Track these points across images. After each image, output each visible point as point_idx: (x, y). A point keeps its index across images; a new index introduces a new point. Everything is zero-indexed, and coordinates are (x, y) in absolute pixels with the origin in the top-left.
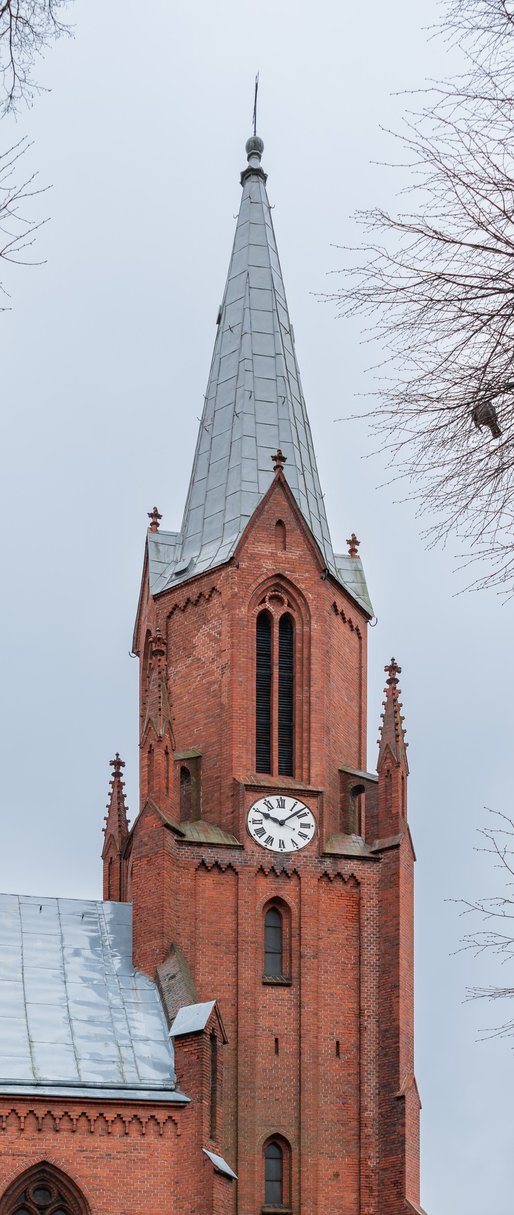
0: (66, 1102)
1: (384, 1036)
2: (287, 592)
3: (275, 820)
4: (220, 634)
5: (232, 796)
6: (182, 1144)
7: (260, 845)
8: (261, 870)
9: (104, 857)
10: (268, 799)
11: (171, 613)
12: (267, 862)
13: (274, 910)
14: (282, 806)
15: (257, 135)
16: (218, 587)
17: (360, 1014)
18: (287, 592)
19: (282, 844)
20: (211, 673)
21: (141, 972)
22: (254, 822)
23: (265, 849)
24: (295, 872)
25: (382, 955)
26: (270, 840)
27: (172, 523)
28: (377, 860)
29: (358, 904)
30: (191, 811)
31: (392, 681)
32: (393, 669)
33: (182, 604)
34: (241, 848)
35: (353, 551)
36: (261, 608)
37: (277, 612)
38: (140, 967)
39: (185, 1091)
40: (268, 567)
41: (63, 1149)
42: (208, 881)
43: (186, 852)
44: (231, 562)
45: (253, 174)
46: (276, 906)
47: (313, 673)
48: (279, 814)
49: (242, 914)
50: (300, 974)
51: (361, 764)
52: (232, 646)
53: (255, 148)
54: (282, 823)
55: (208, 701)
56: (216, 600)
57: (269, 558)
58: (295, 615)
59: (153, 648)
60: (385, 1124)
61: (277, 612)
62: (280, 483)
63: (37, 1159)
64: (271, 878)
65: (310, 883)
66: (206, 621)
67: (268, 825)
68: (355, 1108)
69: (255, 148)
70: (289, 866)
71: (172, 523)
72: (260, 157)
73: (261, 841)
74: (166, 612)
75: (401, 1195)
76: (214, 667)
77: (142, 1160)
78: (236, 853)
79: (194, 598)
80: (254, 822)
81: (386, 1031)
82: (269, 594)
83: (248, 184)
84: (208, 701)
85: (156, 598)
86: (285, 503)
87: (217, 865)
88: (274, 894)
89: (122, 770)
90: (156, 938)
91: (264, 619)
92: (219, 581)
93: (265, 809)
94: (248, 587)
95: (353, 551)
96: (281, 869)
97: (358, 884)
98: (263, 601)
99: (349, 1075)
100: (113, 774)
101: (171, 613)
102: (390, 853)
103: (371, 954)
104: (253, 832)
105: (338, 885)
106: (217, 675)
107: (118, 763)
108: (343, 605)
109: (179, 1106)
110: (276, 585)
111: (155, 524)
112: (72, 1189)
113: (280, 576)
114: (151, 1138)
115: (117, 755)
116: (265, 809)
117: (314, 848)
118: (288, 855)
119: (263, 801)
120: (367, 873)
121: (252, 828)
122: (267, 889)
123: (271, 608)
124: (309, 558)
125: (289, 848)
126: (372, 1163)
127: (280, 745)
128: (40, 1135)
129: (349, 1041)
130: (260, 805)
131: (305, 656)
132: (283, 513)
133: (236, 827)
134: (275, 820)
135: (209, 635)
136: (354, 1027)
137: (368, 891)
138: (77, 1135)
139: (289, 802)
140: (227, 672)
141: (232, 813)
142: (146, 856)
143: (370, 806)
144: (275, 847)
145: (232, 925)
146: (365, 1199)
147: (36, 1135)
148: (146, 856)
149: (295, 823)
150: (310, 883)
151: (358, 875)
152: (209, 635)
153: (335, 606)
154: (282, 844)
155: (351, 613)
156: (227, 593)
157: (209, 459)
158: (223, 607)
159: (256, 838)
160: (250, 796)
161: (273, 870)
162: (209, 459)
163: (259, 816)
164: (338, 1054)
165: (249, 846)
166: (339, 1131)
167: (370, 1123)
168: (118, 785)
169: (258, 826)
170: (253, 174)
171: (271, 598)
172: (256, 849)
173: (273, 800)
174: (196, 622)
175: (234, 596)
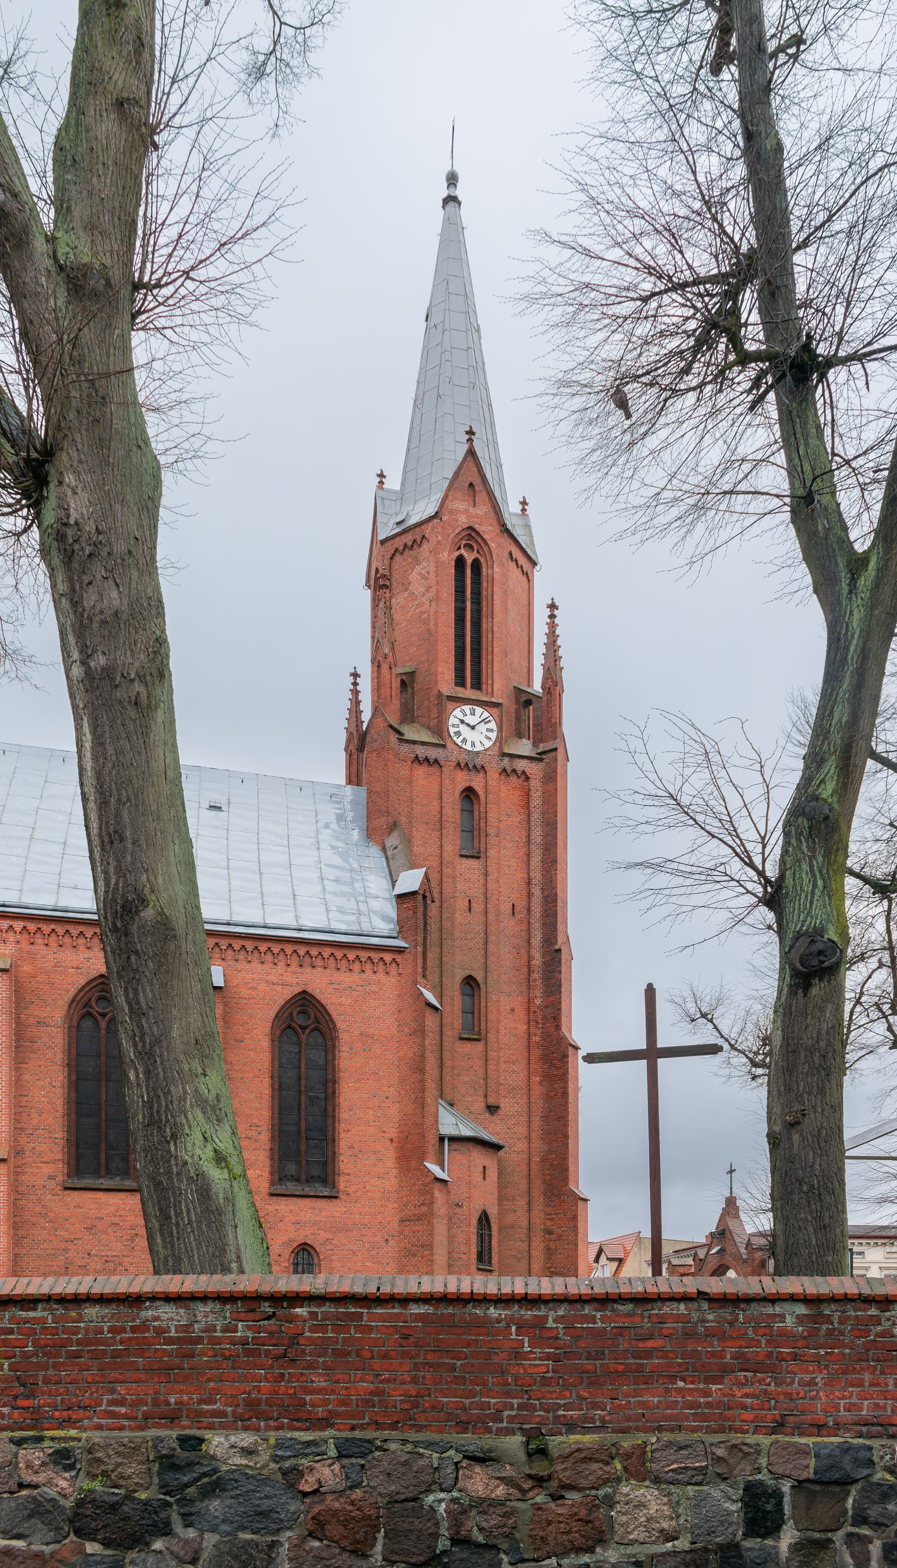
2: (477, 541)
3: (468, 725)
6: (403, 981)
8: (459, 764)
13: (467, 797)
14: (473, 713)
17: (529, 883)
18: (477, 541)
19: (473, 744)
22: (453, 726)
24: (483, 767)
25: (546, 835)
26: (465, 741)
27: (393, 483)
28: (541, 760)
29: (528, 794)
30: (408, 715)
31: (552, 617)
32: (553, 606)
33: (401, 548)
35: (524, 510)
36: (457, 553)
37: (469, 557)
39: (405, 939)
40: (463, 521)
41: (319, 981)
42: (420, 772)
43: (405, 748)
44: (436, 515)
45: (451, 200)
46: (469, 794)
51: (529, 683)
53: (452, 179)
54: (473, 728)
57: (465, 512)
58: (482, 560)
59: (380, 583)
61: (469, 557)
62: (471, 453)
63: (298, 989)
64: (465, 772)
66: (418, 563)
67: (463, 729)
68: (525, 958)
69: (452, 179)
70: (478, 762)
71: (393, 483)
73: (458, 741)
75: (558, 1027)
77: (375, 992)
78: (441, 750)
79: (410, 543)
80: (453, 726)
82: (464, 542)
83: (447, 208)
85: (383, 542)
86: (475, 469)
89: (358, 680)
91: (460, 562)
92: (427, 530)
95: (524, 510)
96: (471, 765)
97: (527, 778)
98: (459, 548)
102: (550, 755)
103: (537, 834)
105: (513, 779)
107: (355, 675)
108: (517, 554)
109: (399, 951)
110: (470, 535)
111: (381, 483)
113: (471, 528)
114: (381, 976)
116: (461, 716)
117: (496, 749)
118: (478, 753)
120: (534, 770)
121: (452, 730)
122: (462, 780)
123: (465, 554)
124: (492, 514)
125: (479, 748)
126: (538, 1002)
127: (472, 662)
129: (521, 905)
130: (457, 712)
132: (473, 478)
133: (440, 729)
134: (468, 725)
135: (420, 574)
136: (524, 893)
139: (479, 710)
143: (535, 716)
144: (468, 747)
149: (482, 728)
151: (528, 771)
152: (420, 574)
153: (511, 554)
154: (473, 744)
155: (522, 561)
159: (455, 738)
160: (450, 705)
165: (450, 746)
168: (355, 692)
169: (456, 730)
170: (451, 200)
171: (465, 546)
172: (455, 747)
173: (467, 708)
175: (439, 543)
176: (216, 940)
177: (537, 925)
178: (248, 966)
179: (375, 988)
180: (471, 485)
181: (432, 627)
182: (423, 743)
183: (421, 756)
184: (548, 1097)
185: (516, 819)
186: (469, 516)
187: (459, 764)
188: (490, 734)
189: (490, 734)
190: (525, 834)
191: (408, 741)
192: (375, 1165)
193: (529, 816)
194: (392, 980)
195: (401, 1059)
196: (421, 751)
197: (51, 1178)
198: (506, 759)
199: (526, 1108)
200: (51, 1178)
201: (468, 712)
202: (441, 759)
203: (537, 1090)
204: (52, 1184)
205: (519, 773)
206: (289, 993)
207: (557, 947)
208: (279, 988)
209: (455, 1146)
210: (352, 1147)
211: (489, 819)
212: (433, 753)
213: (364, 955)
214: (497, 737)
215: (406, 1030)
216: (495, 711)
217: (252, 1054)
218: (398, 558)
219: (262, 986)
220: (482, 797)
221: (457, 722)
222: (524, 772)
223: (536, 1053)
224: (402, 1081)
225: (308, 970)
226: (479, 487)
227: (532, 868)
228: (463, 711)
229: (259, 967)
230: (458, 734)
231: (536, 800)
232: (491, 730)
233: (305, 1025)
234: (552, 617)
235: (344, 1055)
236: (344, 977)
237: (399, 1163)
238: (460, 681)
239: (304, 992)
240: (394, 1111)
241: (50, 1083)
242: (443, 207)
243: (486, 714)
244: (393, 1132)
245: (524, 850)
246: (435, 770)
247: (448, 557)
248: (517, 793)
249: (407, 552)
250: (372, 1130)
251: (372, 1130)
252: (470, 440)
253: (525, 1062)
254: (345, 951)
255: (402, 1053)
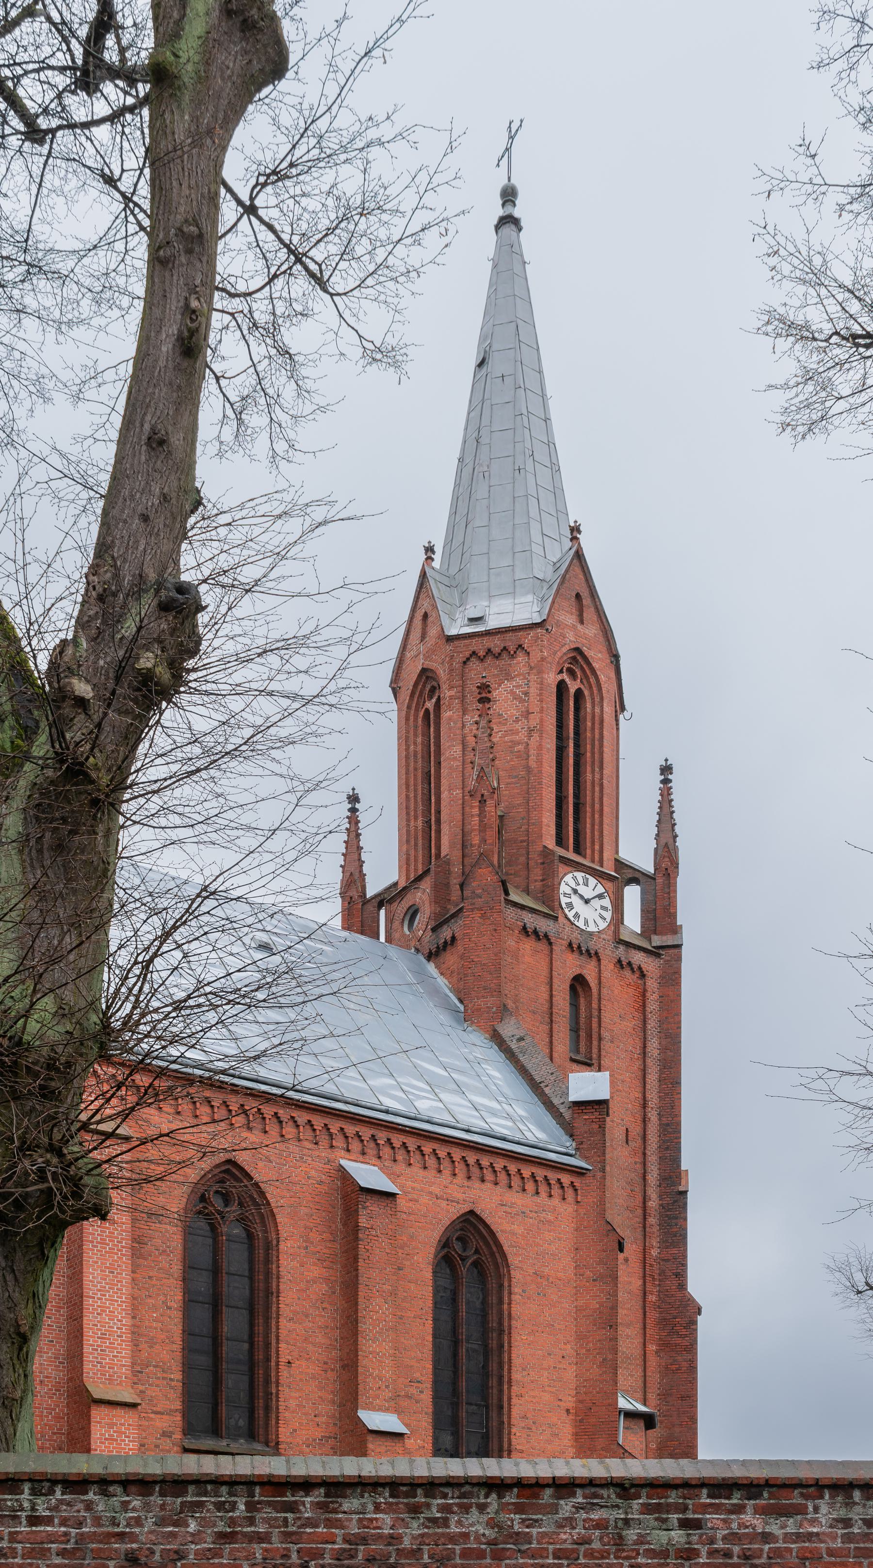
0: (492, 1152)
1: (665, 1130)
3: (581, 897)
4: (526, 694)
5: (543, 863)
6: (582, 1211)
7: (569, 920)
8: (570, 945)
9: (343, 894)
10: (576, 874)
11: (468, 659)
12: (576, 938)
15: (512, 181)
16: (525, 646)
17: (644, 1106)
19: (586, 922)
20: (517, 732)
21: (474, 1027)
23: (572, 924)
24: (596, 953)
25: (663, 1049)
26: (577, 916)
28: (658, 955)
29: (644, 994)
33: (482, 653)
34: (556, 918)
36: (559, 677)
38: (473, 1023)
39: (586, 1158)
40: (571, 639)
41: (492, 1201)
42: (528, 945)
43: (511, 913)
45: (508, 221)
46: (578, 983)
47: (605, 755)
48: (587, 892)
49: (555, 986)
50: (599, 1056)
52: (541, 711)
53: (509, 195)
54: (587, 902)
55: (512, 760)
56: (521, 658)
58: (586, 692)
60: (667, 1216)
61: (573, 686)
62: (579, 556)
63: (465, 1208)
64: (576, 955)
65: (608, 967)
66: (509, 677)
67: (575, 900)
68: (639, 1198)
69: (509, 195)
70: (593, 945)
72: (514, 205)
73: (570, 915)
74: (461, 658)
75: (683, 1286)
76: (518, 726)
77: (549, 1221)
78: (551, 923)
79: (497, 650)
81: (668, 1125)
82: (567, 665)
83: (500, 231)
84: (512, 760)
86: (581, 576)
87: (535, 932)
88: (578, 972)
89: (357, 806)
90: (492, 996)
91: (561, 687)
92: (527, 640)
93: (573, 885)
94: (555, 653)
96: (582, 949)
97: (643, 975)
99: (636, 1163)
100: (349, 810)
101: (468, 659)
102: (671, 951)
103: (653, 1046)
104: (564, 906)
105: (627, 973)
106: (522, 736)
109: (580, 1172)
110: (574, 658)
112: (491, 1243)
113: (577, 650)
114: (556, 1201)
115: (353, 789)
116: (573, 885)
117: (611, 933)
118: (591, 934)
119: (571, 875)
120: (650, 965)
121: (564, 900)
122: (569, 966)
123: (568, 680)
124: (602, 639)
125: (592, 928)
126: (654, 1252)
128: (470, 1183)
129: (636, 1131)
131: (597, 736)
134: (581, 897)
135: (512, 692)
136: (639, 1117)
137: (652, 984)
138: (498, 1188)
139: (592, 881)
140: (536, 736)
141: (542, 880)
142: (480, 909)
144: (580, 924)
145: (546, 996)
146: (649, 1287)
147: (466, 1183)
148: (480, 909)
149: (596, 903)
150: (608, 967)
151: (644, 967)
152: (512, 692)
154: (586, 922)
156: (536, 655)
157: (488, 507)
158: (531, 668)
159: (566, 911)
160: (562, 868)
161: (579, 947)
162: (488, 507)
163: (568, 890)
164: (627, 1142)
165: (561, 919)
166: (628, 1218)
167: (653, 1213)
169: (568, 900)
170: (508, 221)
172: (566, 921)
173: (580, 875)
174: (498, 675)
175: (543, 659)
176: (372, 1131)
177: (653, 1159)
178: (408, 1170)
179: (550, 1217)
180: (578, 596)
181: (533, 764)
182: (533, 911)
183: (530, 927)
184: (667, 1370)
185: (630, 1024)
186: (576, 635)
187: (570, 945)
188: (604, 913)
189: (604, 913)
190: (639, 1044)
191: (515, 904)
192: (549, 1442)
193: (645, 1021)
194: (567, 1209)
195: (579, 1310)
196: (530, 920)
197: (164, 1434)
198: (622, 948)
199: (640, 1383)
200: (164, 1434)
201: (581, 881)
202: (551, 934)
203: (653, 1361)
204: (167, 1443)
205: (635, 967)
206: (455, 1211)
207: (681, 1189)
208: (444, 1203)
209: (632, 1423)
210: (525, 1417)
211: (603, 1019)
212: (544, 925)
213: (540, 1173)
214: (612, 918)
215: (588, 1273)
216: (609, 885)
217: (412, 1286)
218: (474, 664)
219: (425, 1199)
220: (595, 990)
221: (568, 890)
222: (640, 968)
223: (653, 1315)
224: (580, 1337)
225: (477, 1184)
226: (587, 601)
227: (648, 1087)
228: (574, 878)
229: (421, 1173)
230: (570, 906)
231: (652, 1005)
232: (603, 908)
233: (470, 1259)
234: (666, 781)
235: (516, 1298)
236: (515, 1198)
237: (576, 1440)
238: (560, 841)
239: (472, 1212)
240: (570, 1373)
241: (164, 1303)
242: (497, 228)
243: (600, 889)
244: (569, 1402)
245: (638, 1064)
246: (542, 946)
247: (552, 678)
248: (631, 991)
249: (489, 660)
250: (546, 1397)
251: (546, 1397)
252: (574, 539)
253: (639, 1325)
254: (520, 1166)
255: (581, 1302)
